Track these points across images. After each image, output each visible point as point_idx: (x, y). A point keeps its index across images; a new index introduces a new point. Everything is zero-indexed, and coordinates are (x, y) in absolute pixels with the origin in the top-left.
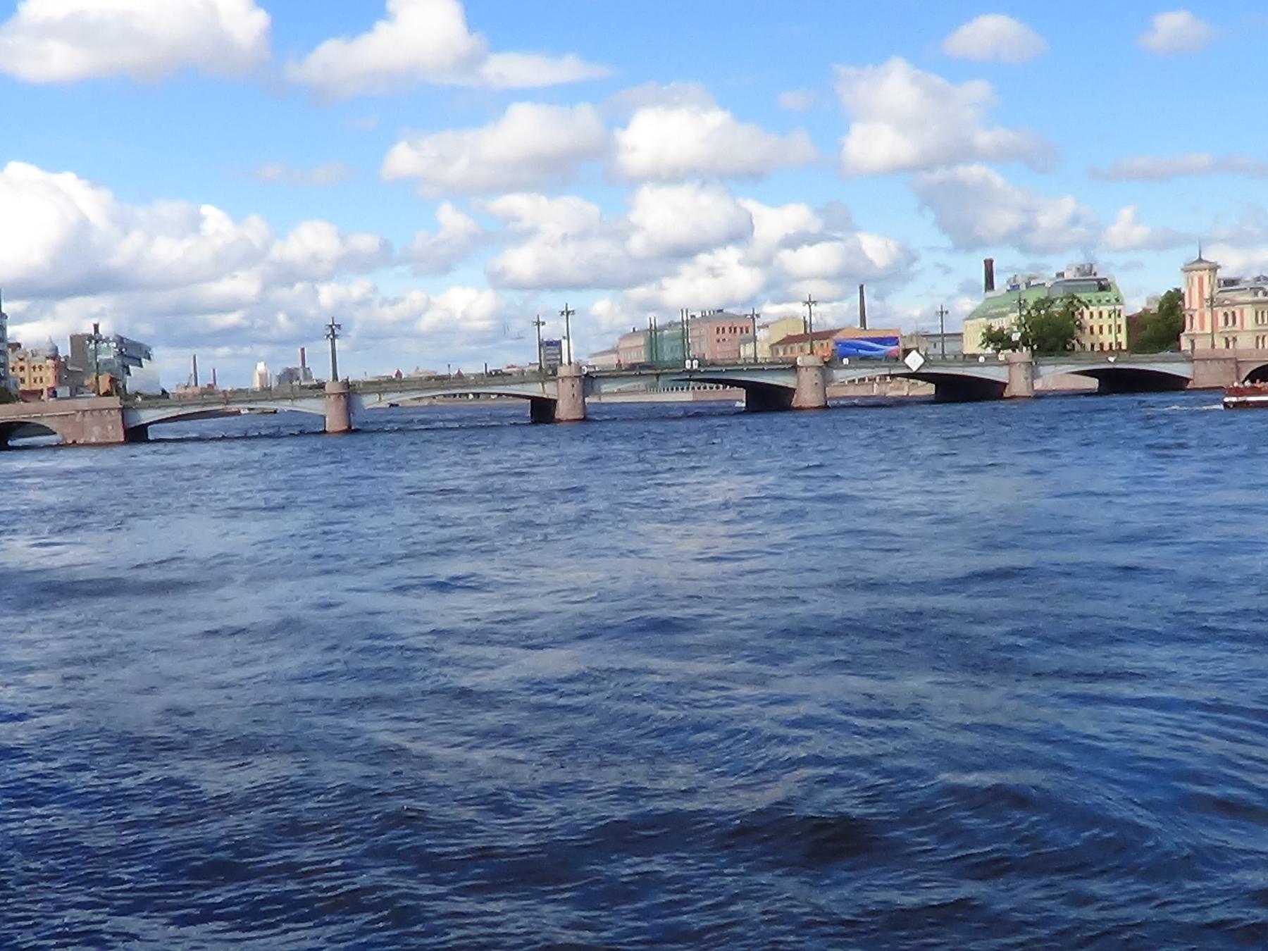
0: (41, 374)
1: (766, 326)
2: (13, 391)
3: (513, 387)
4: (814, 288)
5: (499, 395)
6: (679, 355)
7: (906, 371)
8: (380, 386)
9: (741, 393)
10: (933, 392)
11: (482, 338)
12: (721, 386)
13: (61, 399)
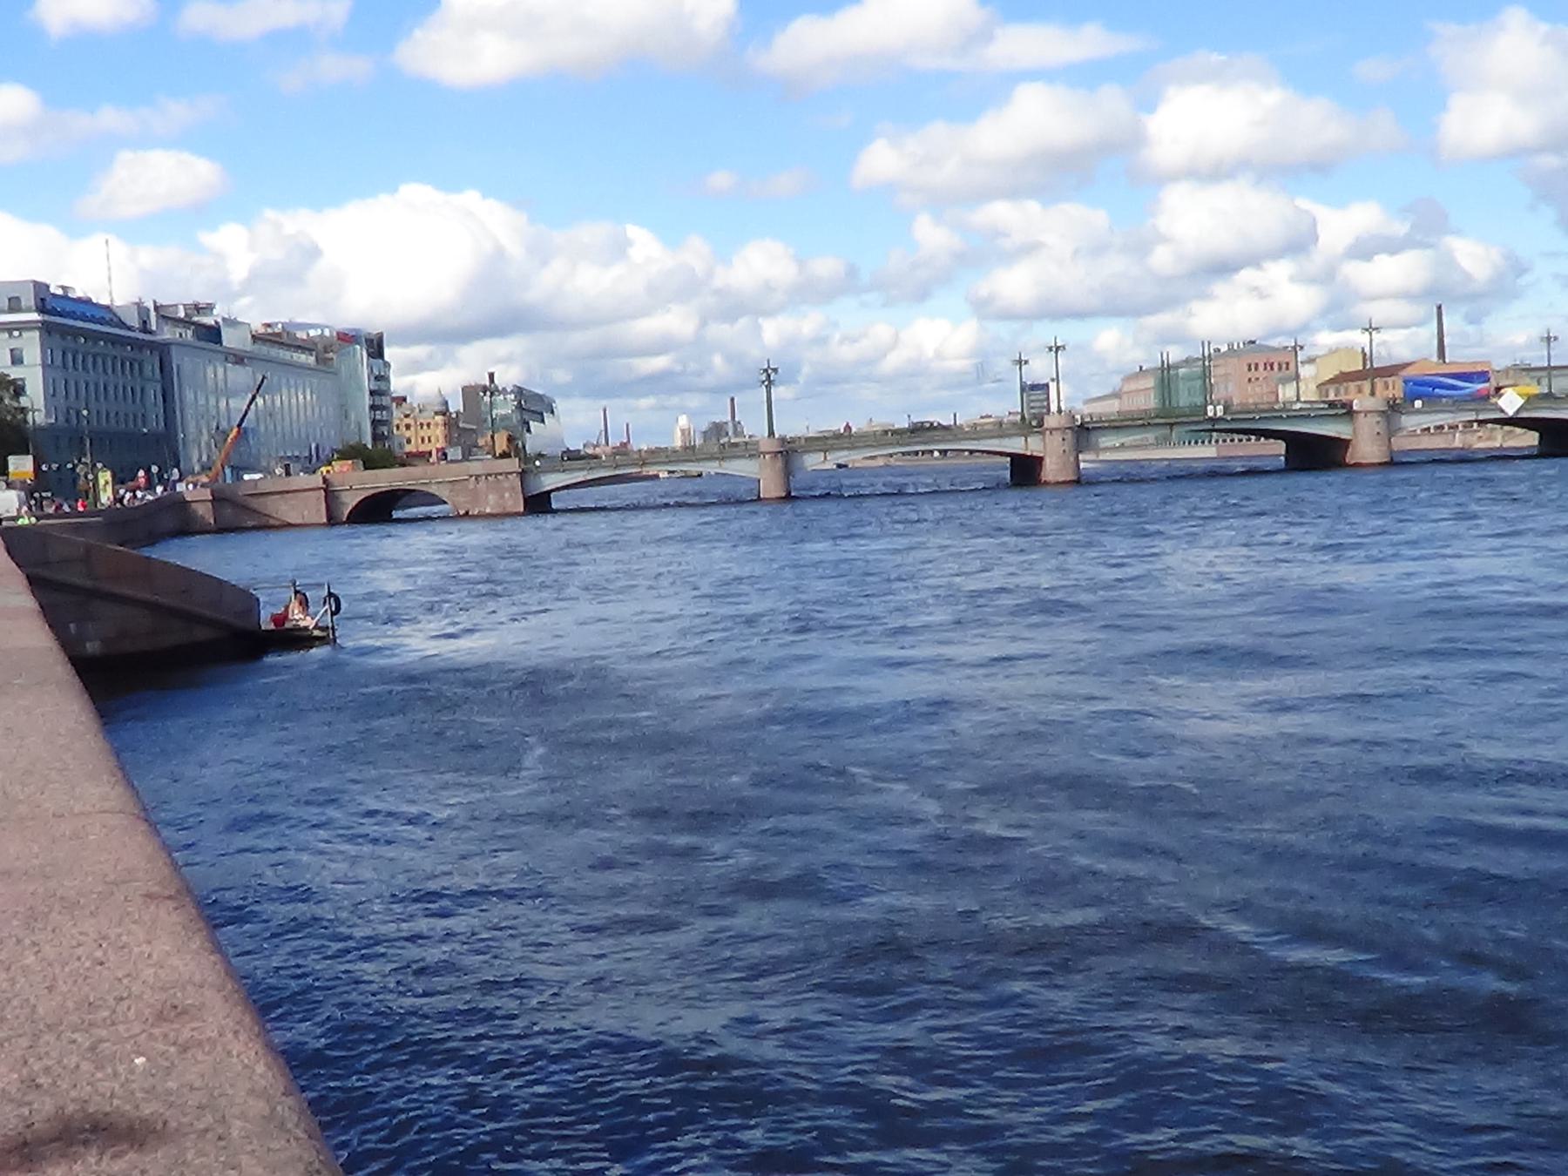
0: (429, 433)
1: (1311, 361)
2: (397, 452)
3: (982, 442)
4: (1378, 311)
5: (971, 452)
6: (1199, 400)
7: (1498, 415)
8: (825, 443)
9: (1280, 447)
10: (1536, 443)
11: (957, 382)
12: (1253, 437)
13: (452, 461)
